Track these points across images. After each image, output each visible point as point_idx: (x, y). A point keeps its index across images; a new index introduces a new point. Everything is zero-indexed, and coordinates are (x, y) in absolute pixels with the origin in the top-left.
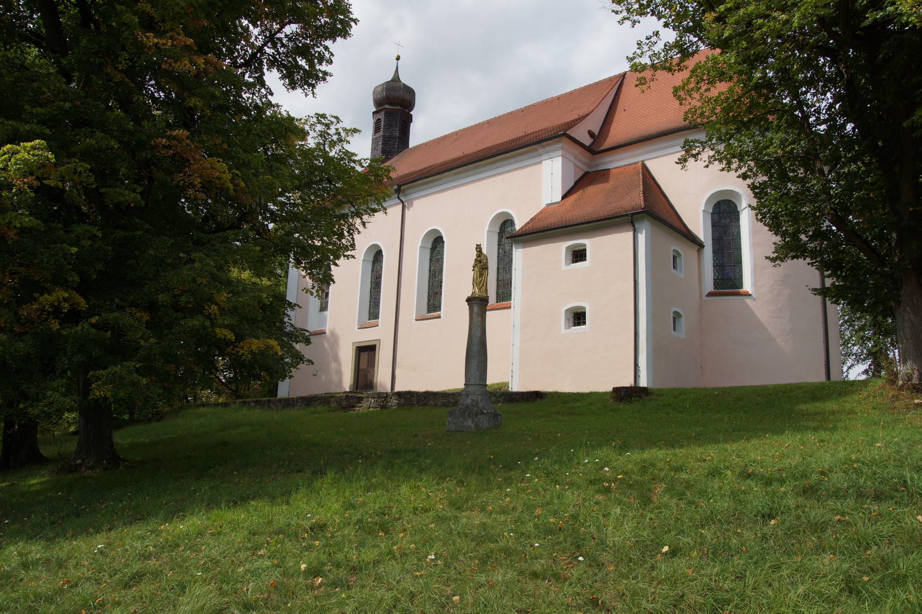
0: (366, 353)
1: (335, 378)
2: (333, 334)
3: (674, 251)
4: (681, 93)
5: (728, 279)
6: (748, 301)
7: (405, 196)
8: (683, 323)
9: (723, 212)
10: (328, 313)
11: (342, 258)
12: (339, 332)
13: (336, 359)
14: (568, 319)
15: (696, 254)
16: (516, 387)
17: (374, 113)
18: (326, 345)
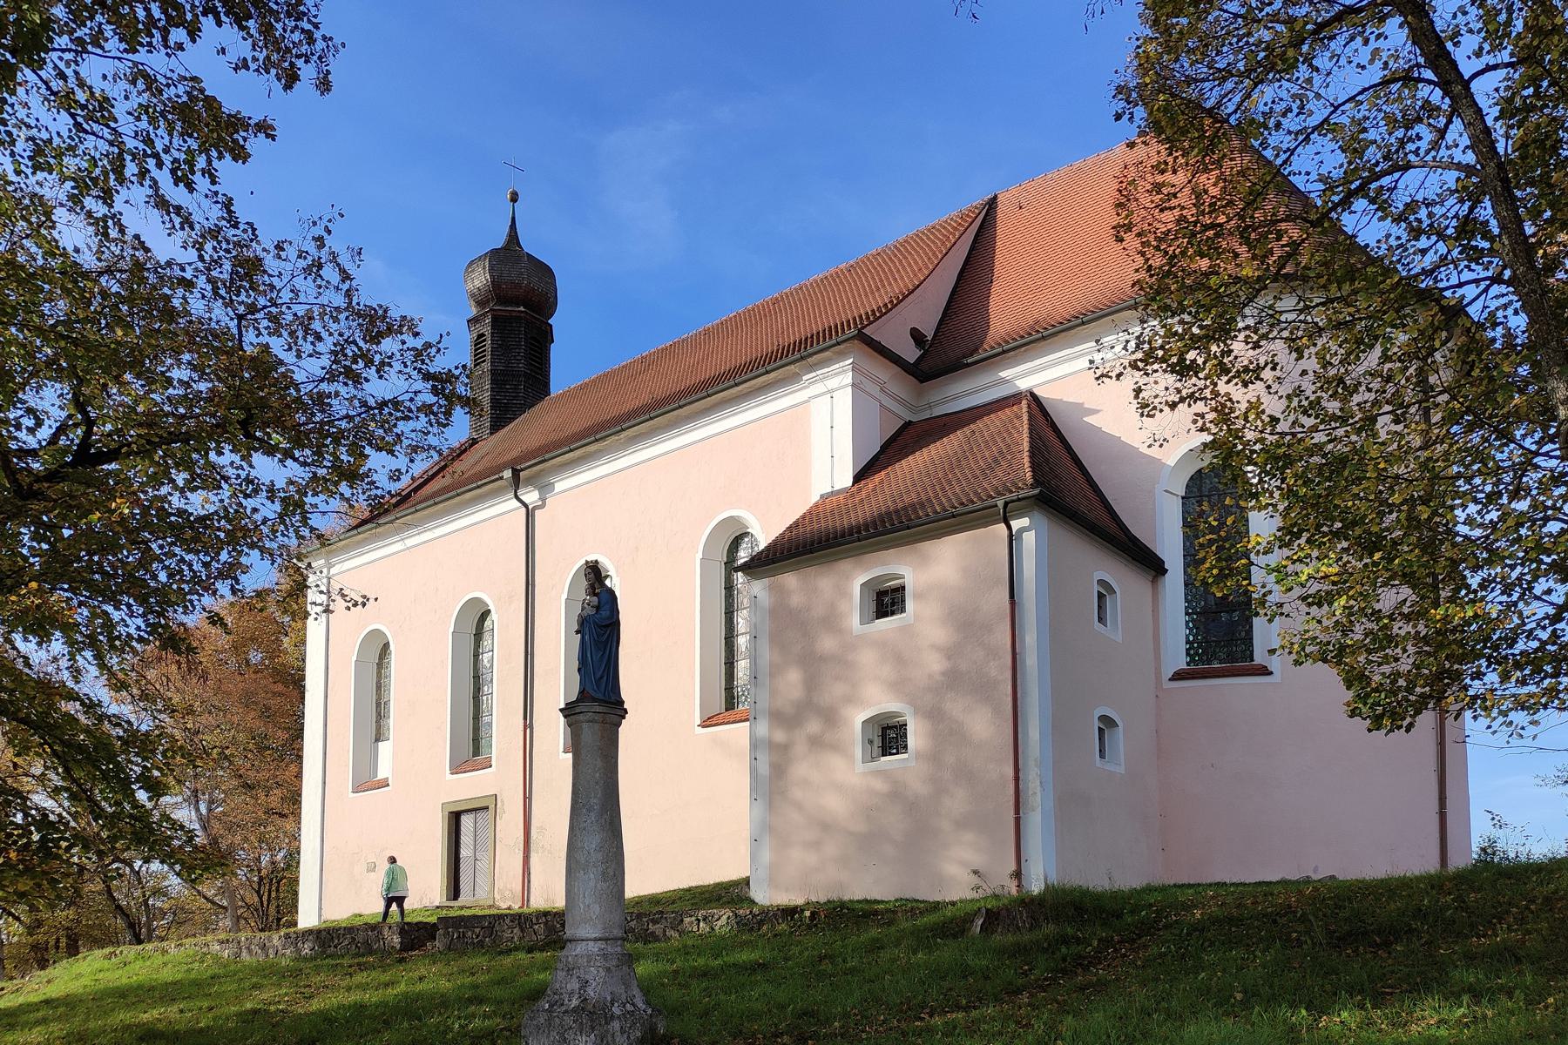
3: (1101, 582)
8: (1119, 739)
14: (871, 742)
17: (473, 321)
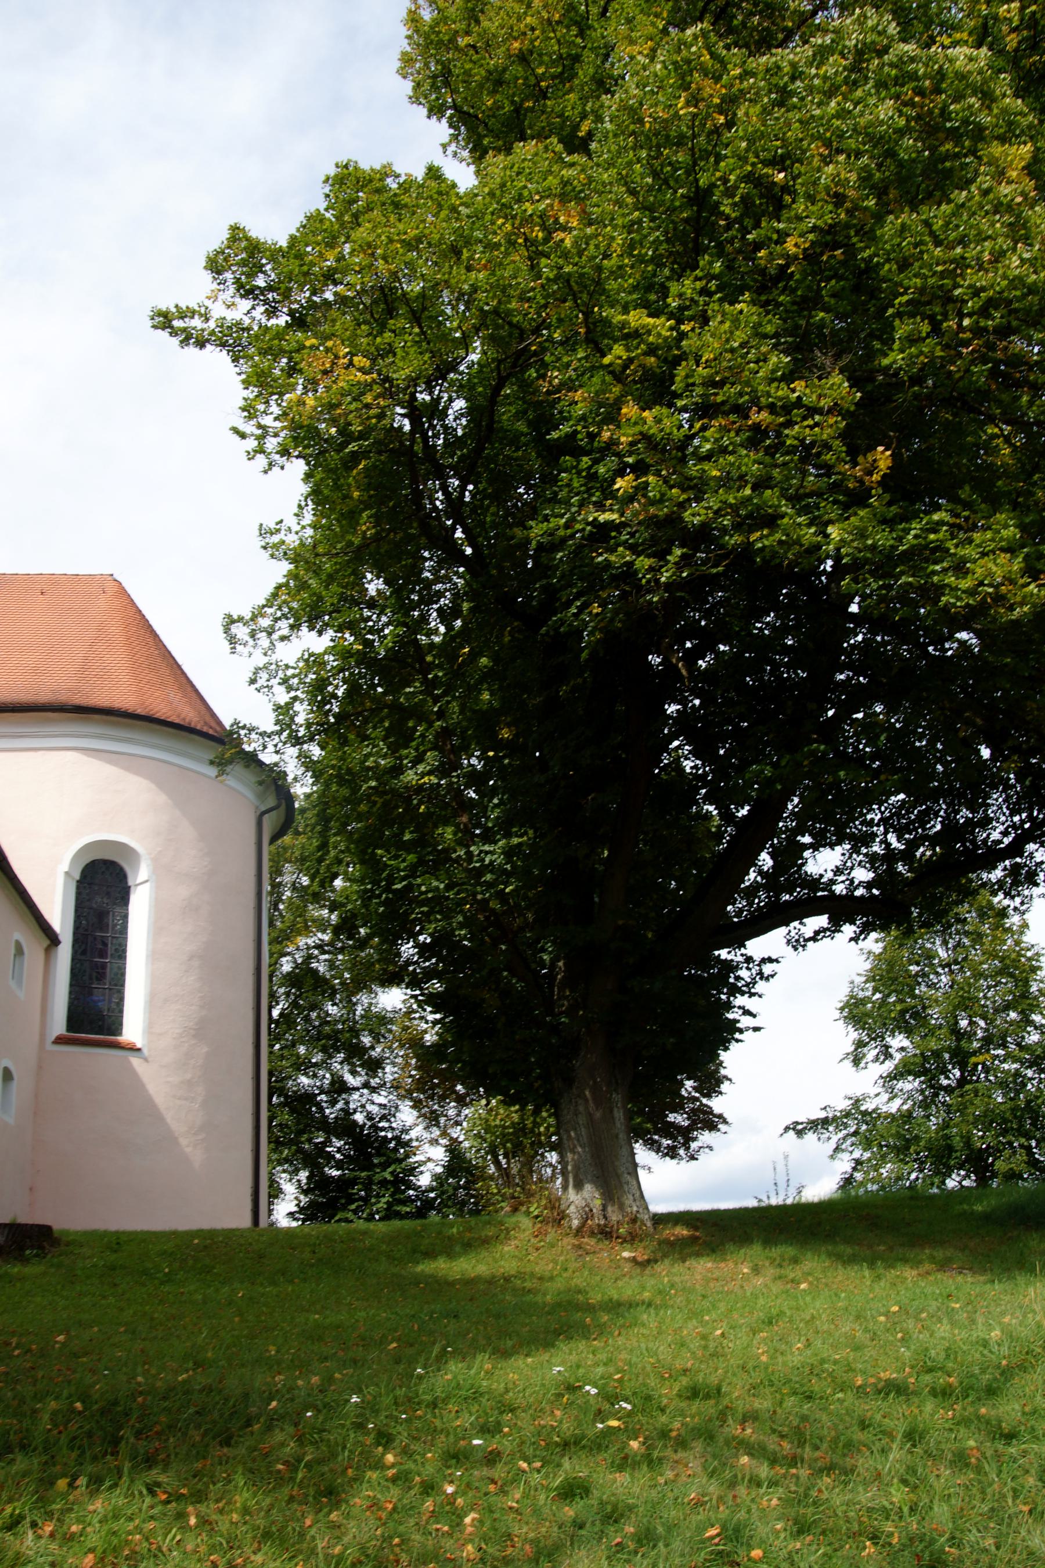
4: (241, 631)
5: (93, 1015)
6: (135, 1061)
9: (102, 882)
11: (854, 1035)
15: (41, 955)
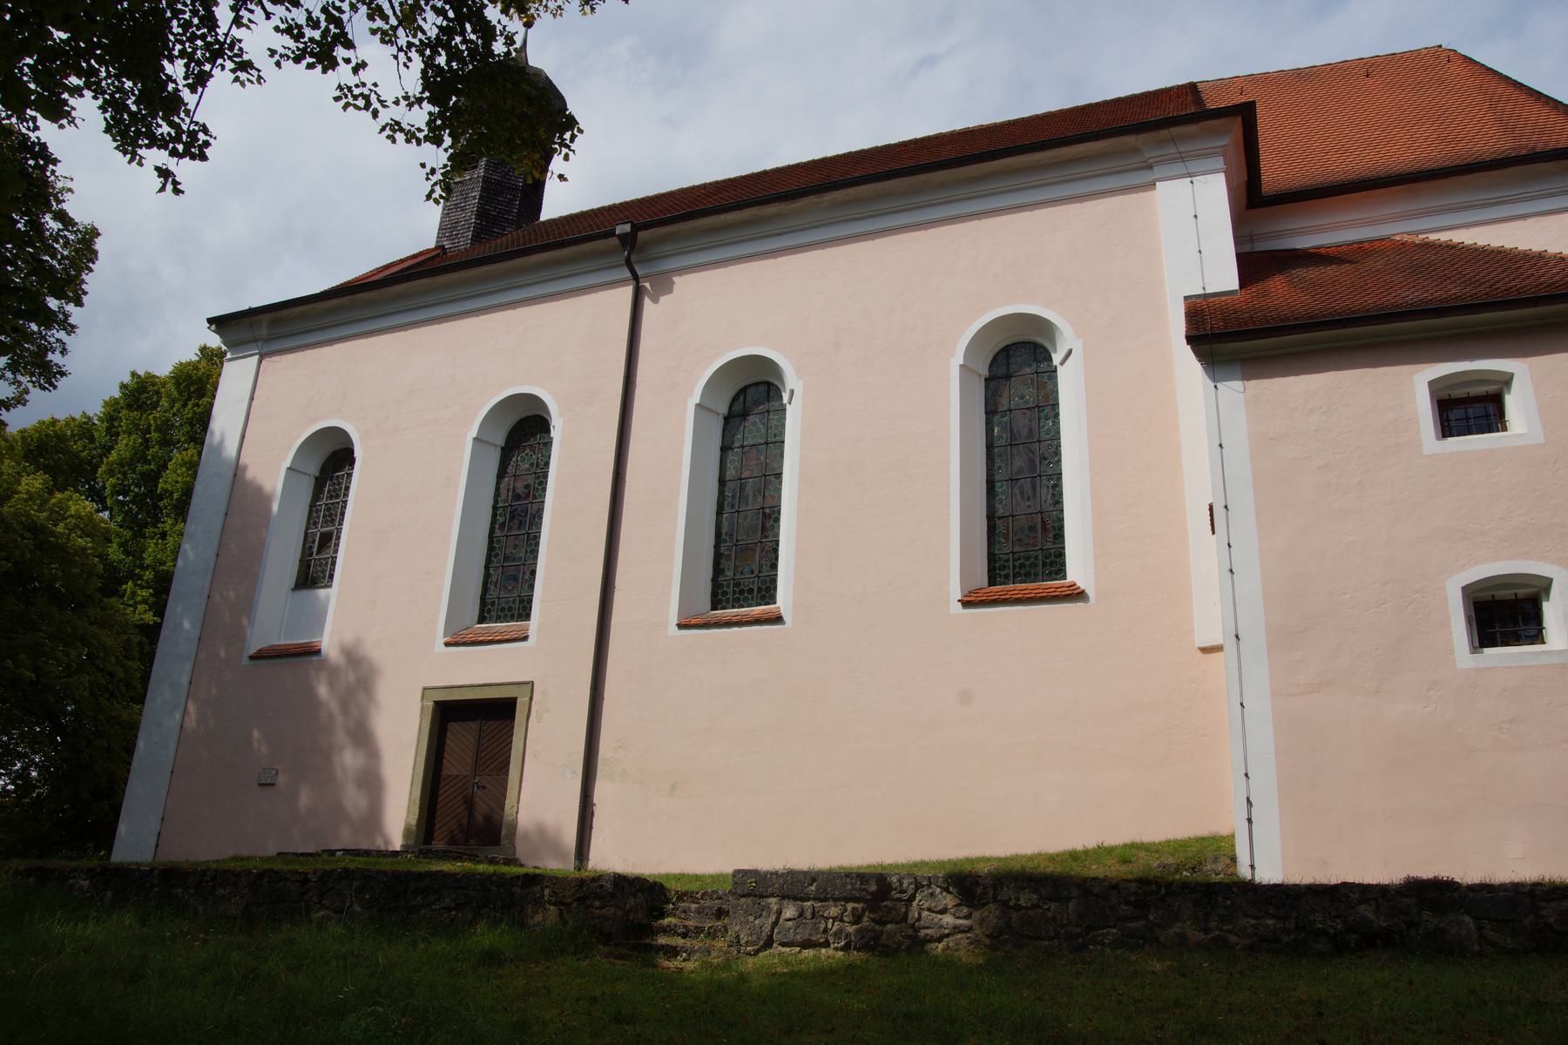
0: (474, 730)
1: (354, 800)
2: (353, 657)
7: (642, 261)
10: (331, 596)
12: (375, 651)
13: (363, 737)
16: (1269, 862)
18: (323, 691)
